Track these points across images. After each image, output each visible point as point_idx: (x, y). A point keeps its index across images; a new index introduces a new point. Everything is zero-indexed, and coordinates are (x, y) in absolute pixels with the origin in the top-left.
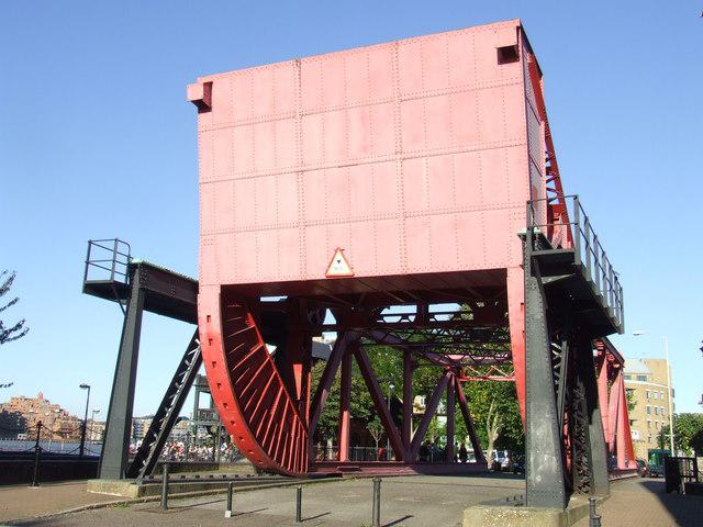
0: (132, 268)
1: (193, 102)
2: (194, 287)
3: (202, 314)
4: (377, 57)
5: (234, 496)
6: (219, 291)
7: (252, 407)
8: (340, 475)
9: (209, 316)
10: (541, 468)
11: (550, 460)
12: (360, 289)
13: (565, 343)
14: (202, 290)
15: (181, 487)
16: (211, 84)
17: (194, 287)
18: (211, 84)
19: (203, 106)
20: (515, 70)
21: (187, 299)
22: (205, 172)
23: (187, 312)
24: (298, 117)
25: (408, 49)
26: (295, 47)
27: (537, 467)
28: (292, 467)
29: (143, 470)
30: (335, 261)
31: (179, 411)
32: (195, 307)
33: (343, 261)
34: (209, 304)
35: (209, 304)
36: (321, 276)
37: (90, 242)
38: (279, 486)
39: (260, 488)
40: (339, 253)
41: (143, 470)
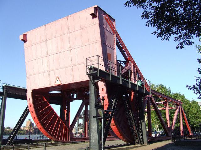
0: (4, 88)
1: (91, 14)
2: (25, 91)
3: (28, 98)
4: (63, 22)
5: (46, 148)
6: (31, 92)
7: (46, 123)
8: (84, 141)
9: (103, 89)
10: (94, 138)
11: (96, 135)
12: (72, 87)
13: (115, 99)
14: (28, 91)
15: (18, 147)
16: (26, 34)
17: (25, 91)
18: (26, 34)
19: (25, 41)
20: (97, 20)
21: (22, 94)
22: (27, 59)
23: (24, 98)
24: (69, 33)
25: (70, 18)
26: (44, 22)
27: (93, 138)
28: (63, 140)
29: (8, 143)
30: (57, 81)
31: (20, 127)
32: (26, 96)
33: (59, 81)
34: (29, 95)
35: (29, 95)
36: (54, 85)
37: (87, 59)
38: (57, 146)
39: (50, 146)
40: (57, 78)
41: (8, 143)
